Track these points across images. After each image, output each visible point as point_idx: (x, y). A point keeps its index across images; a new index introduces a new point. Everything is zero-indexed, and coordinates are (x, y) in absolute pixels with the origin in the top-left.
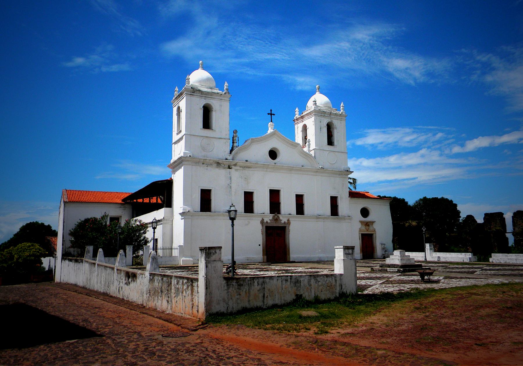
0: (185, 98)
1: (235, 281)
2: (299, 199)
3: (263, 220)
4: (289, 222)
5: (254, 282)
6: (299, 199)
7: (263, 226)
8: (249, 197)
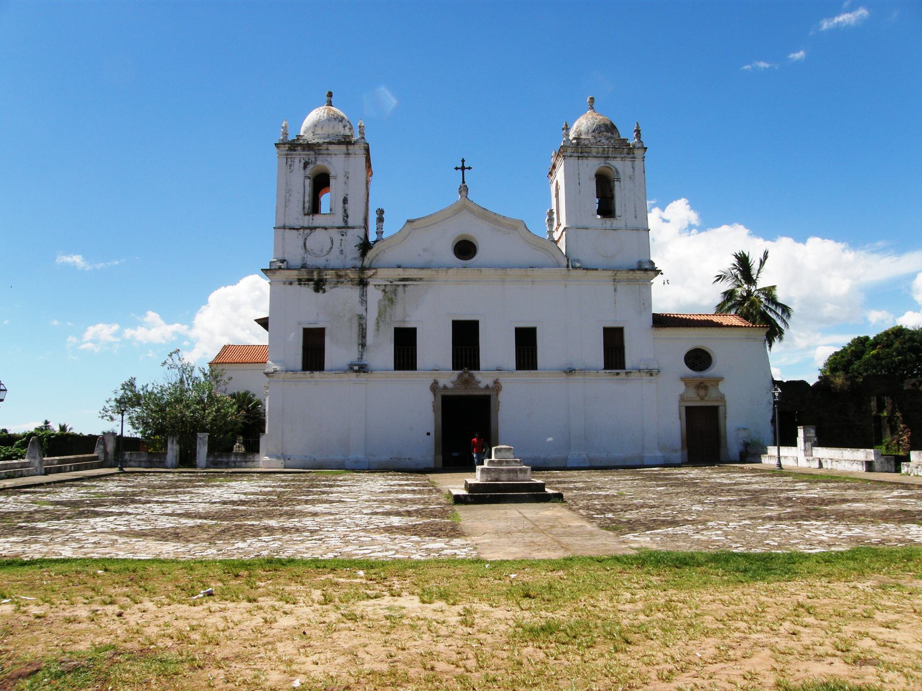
4: (497, 386)
7: (435, 395)
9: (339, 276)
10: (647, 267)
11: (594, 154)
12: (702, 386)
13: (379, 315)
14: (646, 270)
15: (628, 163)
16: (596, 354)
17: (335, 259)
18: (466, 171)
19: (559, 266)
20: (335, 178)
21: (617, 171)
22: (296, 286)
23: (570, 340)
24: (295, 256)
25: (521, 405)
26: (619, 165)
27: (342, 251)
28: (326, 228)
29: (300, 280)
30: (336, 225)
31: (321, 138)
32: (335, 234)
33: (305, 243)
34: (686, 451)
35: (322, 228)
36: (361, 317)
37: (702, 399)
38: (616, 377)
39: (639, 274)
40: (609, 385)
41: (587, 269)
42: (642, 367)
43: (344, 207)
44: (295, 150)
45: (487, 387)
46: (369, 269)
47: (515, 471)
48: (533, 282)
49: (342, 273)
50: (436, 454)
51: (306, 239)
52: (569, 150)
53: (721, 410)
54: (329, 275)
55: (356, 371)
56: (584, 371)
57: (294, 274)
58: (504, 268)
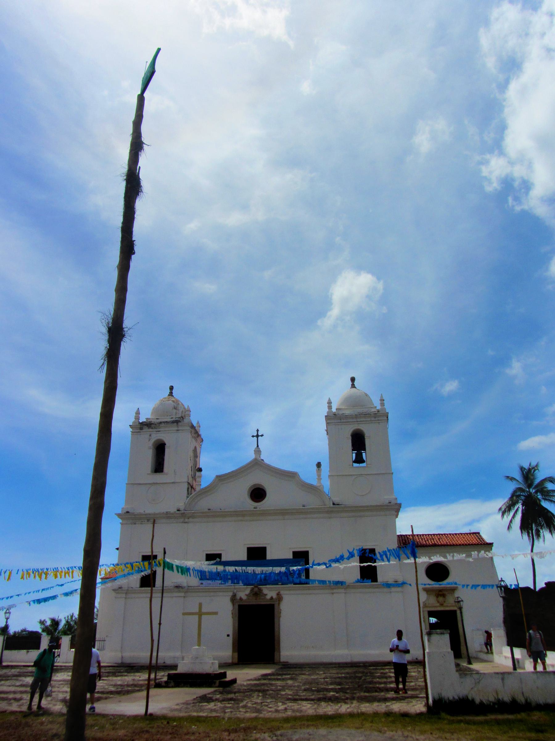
7: (233, 605)
12: (440, 594)
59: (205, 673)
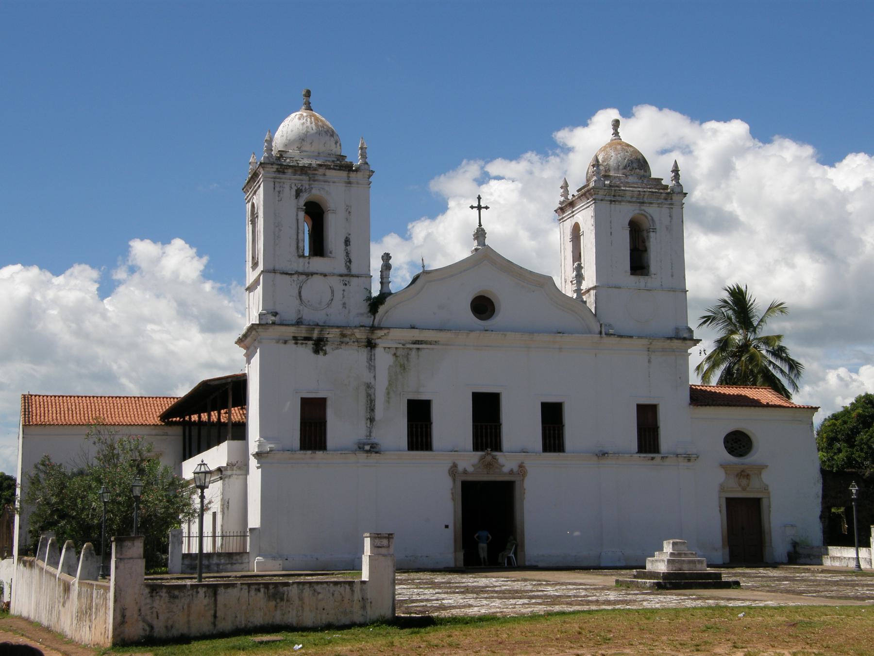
0: (262, 186)
1: (164, 590)
2: (552, 416)
3: (455, 466)
4: (522, 470)
5: (197, 592)
6: (552, 416)
7: (454, 480)
8: (419, 414)
9: (343, 335)
10: (686, 335)
11: (628, 198)
12: (743, 474)
13: (390, 385)
14: (684, 339)
15: (665, 210)
16: (630, 437)
17: (336, 314)
18: (483, 211)
19: (590, 332)
20: (334, 212)
21: (653, 219)
22: (291, 345)
23: (600, 420)
24: (289, 309)
25: (548, 493)
26: (656, 212)
27: (344, 304)
28: (325, 275)
29: (295, 338)
30: (337, 271)
31: (309, 157)
32: (336, 283)
33: (300, 293)
34: (727, 550)
35: (321, 274)
36: (369, 386)
37: (744, 489)
38: (651, 462)
39: (677, 343)
40: (642, 468)
41: (621, 336)
42: (679, 451)
43: (346, 249)
44: (284, 173)
45: (511, 472)
46: (381, 328)
47: (693, 562)
48: (560, 349)
49: (348, 332)
50: (455, 551)
51: (301, 287)
52: (601, 192)
53: (765, 503)
54: (332, 335)
55: (367, 452)
56: (617, 454)
57: (291, 331)
58: (531, 332)
59: (685, 117)
